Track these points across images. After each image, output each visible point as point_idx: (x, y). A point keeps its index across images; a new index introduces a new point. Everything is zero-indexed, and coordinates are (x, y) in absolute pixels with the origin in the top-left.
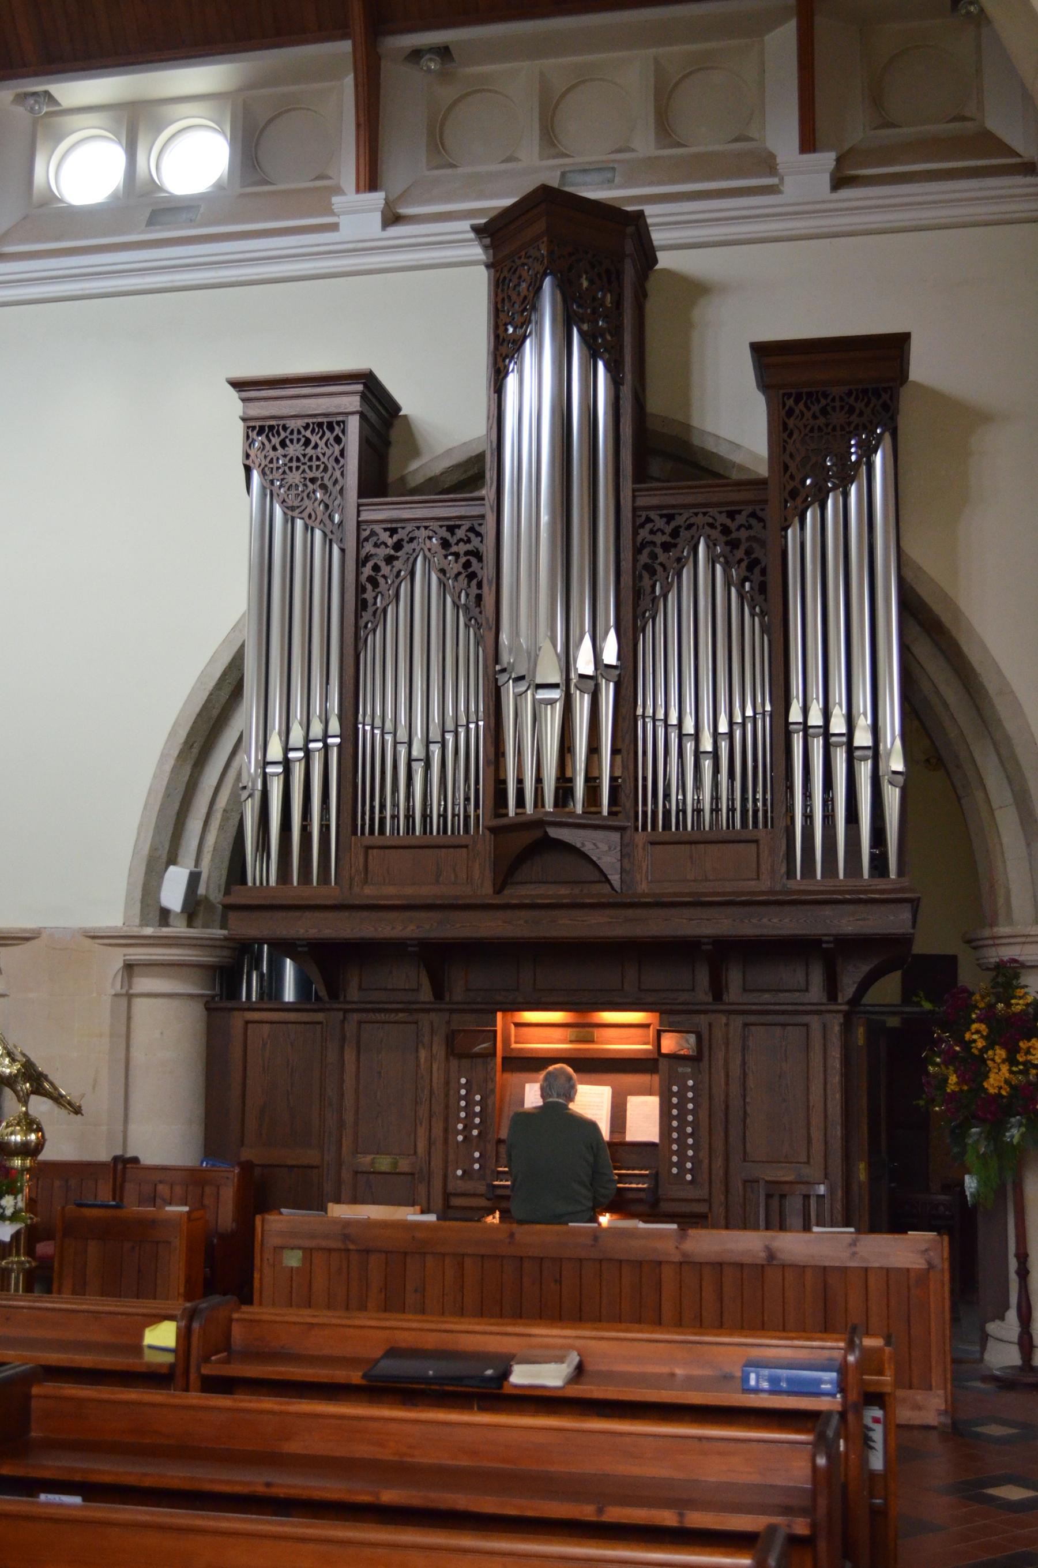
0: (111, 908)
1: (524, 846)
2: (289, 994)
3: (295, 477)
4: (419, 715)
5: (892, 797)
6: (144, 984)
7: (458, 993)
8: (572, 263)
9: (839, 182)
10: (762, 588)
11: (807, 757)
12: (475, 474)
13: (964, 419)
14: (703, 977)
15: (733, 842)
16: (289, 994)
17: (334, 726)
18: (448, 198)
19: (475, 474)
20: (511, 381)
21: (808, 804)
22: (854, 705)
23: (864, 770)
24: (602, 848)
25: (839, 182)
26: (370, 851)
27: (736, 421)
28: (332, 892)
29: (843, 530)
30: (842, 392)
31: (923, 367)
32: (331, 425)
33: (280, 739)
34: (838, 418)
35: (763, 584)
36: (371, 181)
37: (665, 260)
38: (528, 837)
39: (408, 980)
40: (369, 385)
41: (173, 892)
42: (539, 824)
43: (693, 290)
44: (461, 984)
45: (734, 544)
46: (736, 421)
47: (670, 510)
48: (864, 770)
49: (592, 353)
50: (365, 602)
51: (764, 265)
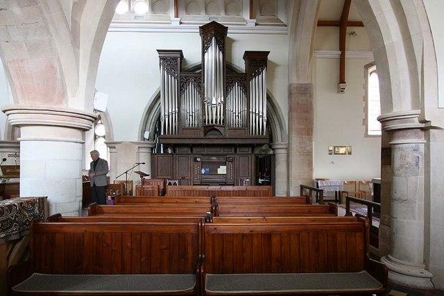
0: (135, 137)
1: (209, 129)
2: (162, 152)
3: (169, 67)
4: (191, 107)
5: (265, 123)
6: (141, 150)
7: (194, 152)
8: (214, 34)
9: (256, 24)
10: (246, 90)
11: (252, 116)
12: (201, 67)
13: (275, 65)
14: (250, 149)
15: (62, 126)
16: (162, 152)
17: (177, 110)
18: (190, 20)
19: (201, 67)
20: (206, 54)
21: (253, 124)
22: (259, 107)
23: (261, 119)
24: (222, 130)
25: (256, 24)
26: (370, 133)
27: (240, 64)
28: (177, 136)
29: (257, 83)
30: (257, 60)
31: (270, 57)
32: (175, 59)
33: (168, 109)
34: (258, 64)
35: (246, 90)
36: (177, 16)
37: (228, 35)
38: (210, 128)
39: (187, 150)
40: (181, 51)
41: (147, 135)
42: (213, 126)
43: (232, 41)
44: (195, 150)
45: (241, 83)
46: (240, 64)
47: (231, 77)
48: (261, 119)
49: (220, 50)
50: (181, 89)
51: (247, 37)
